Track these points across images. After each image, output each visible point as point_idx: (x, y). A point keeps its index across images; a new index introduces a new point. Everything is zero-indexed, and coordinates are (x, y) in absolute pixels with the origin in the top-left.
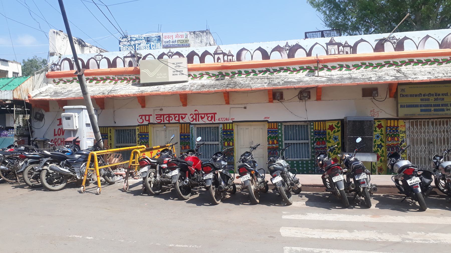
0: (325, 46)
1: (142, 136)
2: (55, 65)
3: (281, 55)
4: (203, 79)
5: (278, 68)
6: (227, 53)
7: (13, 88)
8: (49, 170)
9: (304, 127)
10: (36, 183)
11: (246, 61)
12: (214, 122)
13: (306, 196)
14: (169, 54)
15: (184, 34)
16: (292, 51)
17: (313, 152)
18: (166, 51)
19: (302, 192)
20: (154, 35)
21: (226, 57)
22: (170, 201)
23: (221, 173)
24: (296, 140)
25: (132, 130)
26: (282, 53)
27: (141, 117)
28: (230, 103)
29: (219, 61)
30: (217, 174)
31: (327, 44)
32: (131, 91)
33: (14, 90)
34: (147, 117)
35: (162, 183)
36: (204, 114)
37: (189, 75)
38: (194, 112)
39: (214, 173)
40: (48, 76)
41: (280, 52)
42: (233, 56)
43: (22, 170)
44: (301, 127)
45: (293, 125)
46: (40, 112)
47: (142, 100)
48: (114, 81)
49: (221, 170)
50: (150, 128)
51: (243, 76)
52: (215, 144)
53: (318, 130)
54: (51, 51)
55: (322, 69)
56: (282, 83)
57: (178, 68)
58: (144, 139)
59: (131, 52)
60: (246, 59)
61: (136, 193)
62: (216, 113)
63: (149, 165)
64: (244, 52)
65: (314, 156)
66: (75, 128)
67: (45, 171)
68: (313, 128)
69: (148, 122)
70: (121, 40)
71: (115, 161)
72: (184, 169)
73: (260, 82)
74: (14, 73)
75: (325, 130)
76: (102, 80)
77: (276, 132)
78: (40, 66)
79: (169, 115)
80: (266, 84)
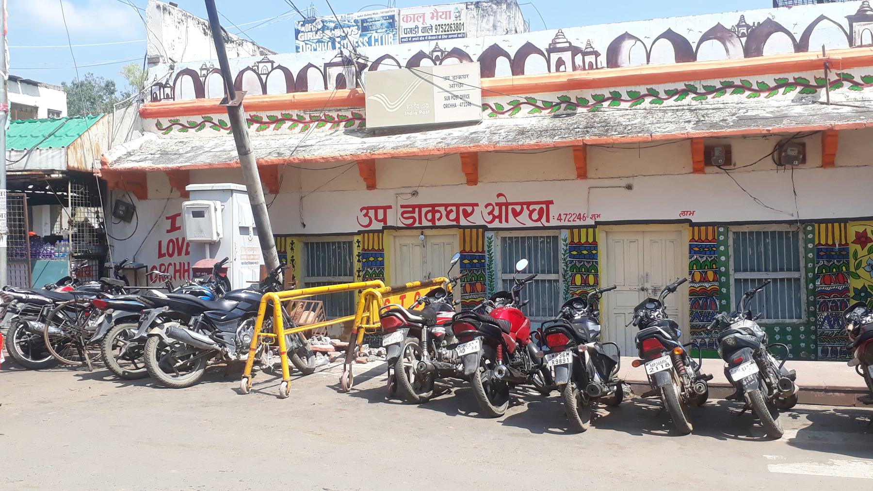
0: (845, 24)
1: (367, 258)
2: (161, 86)
3: (727, 51)
4: (520, 114)
5: (717, 83)
6: (583, 47)
7: (66, 141)
8: (164, 336)
9: (788, 238)
10: (130, 369)
11: (633, 65)
12: (547, 224)
13: (807, 418)
14: (435, 54)
15: (452, 8)
16: (756, 37)
17: (814, 303)
18: (427, 47)
19: (797, 406)
20: (378, 14)
21: (579, 59)
22: (460, 419)
23: (592, 352)
24: (766, 270)
25: (344, 243)
26: (728, 44)
27: (365, 211)
28: (590, 175)
29: (562, 68)
30: (583, 354)
31: (852, 19)
32: (345, 147)
33: (68, 148)
34: (381, 213)
35: (437, 373)
36: (522, 204)
37: (485, 106)
38: (494, 200)
39: (576, 351)
40: (144, 114)
41: (722, 40)
42: (597, 54)
43: (99, 337)
44: (781, 238)
45: (758, 233)
46: (127, 200)
47: (369, 170)
48: (301, 125)
49: (591, 345)
50: (388, 240)
51: (624, 105)
52: (550, 281)
53: (827, 244)
54: (152, 53)
55: (837, 84)
56: (734, 121)
57: (456, 88)
58: (374, 265)
59: (341, 53)
60: (632, 62)
61: (374, 396)
62: (551, 202)
63: (405, 326)
64: (627, 44)
65: (814, 314)
66: (215, 238)
67: (156, 339)
68: (812, 241)
69: (382, 224)
70: (299, 28)
71: (308, 319)
72: (493, 341)
73: (672, 120)
74: (50, 112)
75: (847, 244)
76: (272, 123)
77: (711, 250)
78: (100, 97)
79: (433, 206)
80: (691, 125)
